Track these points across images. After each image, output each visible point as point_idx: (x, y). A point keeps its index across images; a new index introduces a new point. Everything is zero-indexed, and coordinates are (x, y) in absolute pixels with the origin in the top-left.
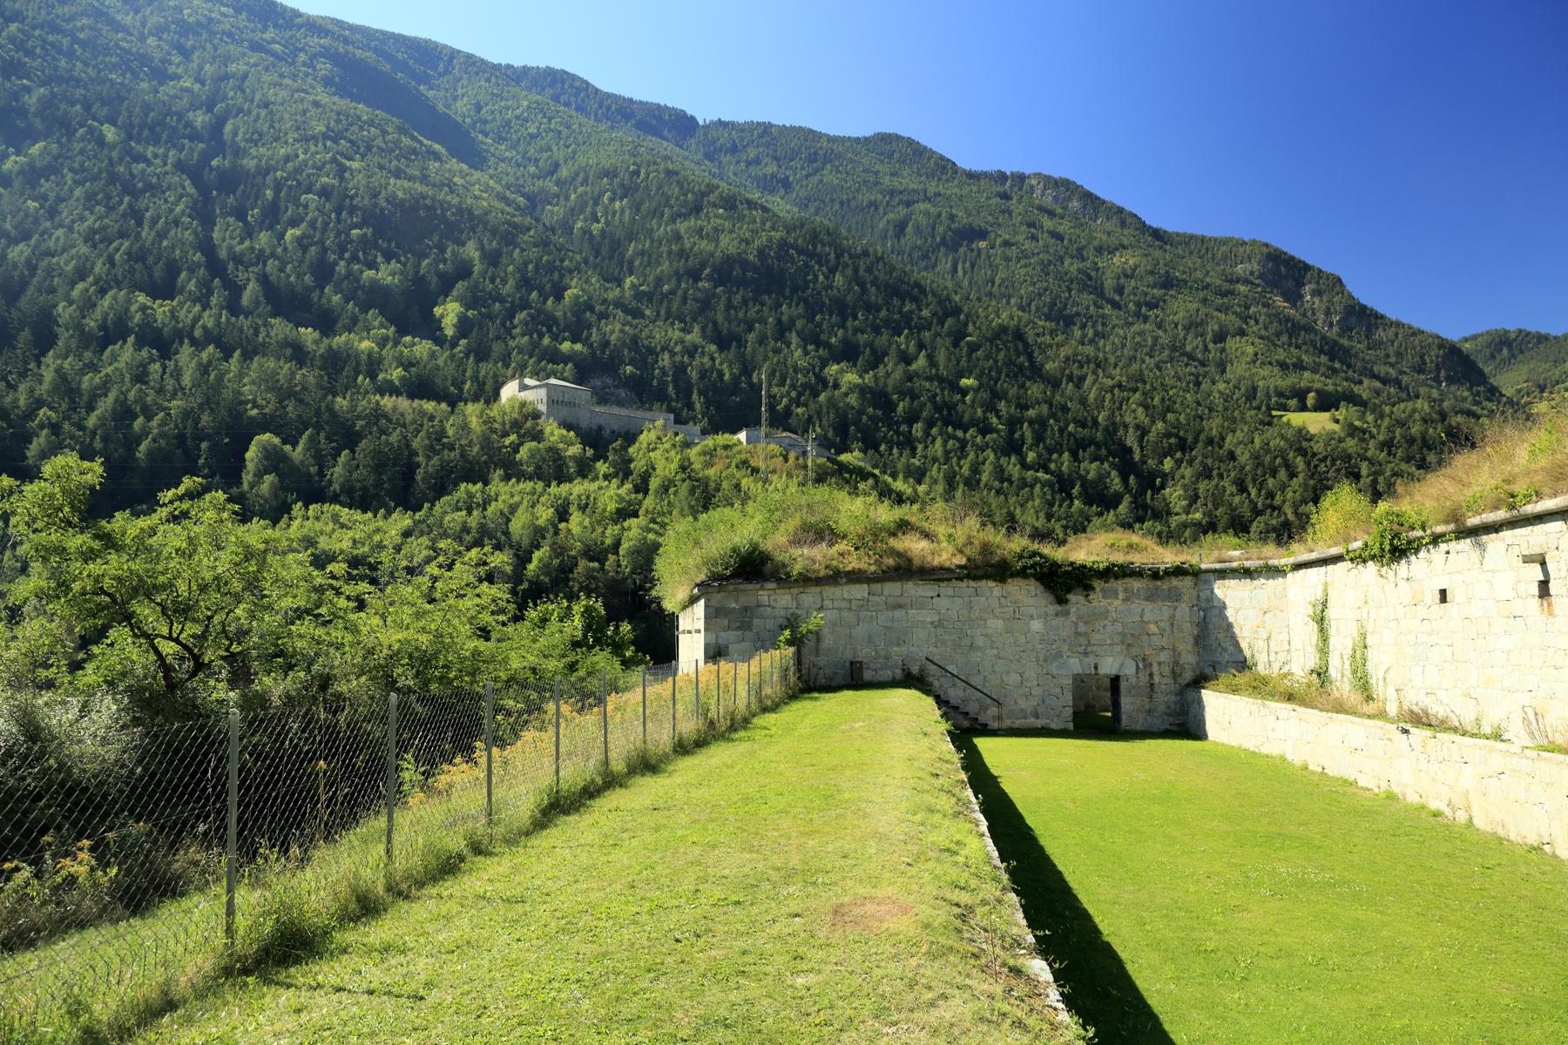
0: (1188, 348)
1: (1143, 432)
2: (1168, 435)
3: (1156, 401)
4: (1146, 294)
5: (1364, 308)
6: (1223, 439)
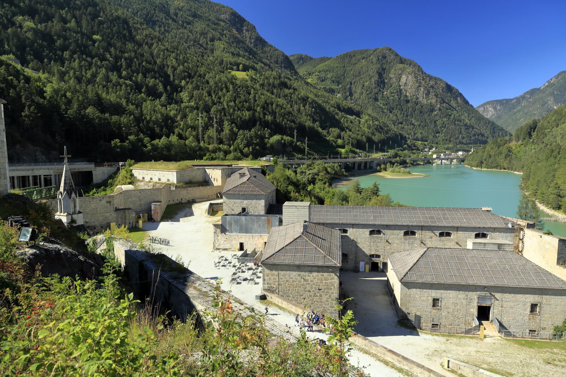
0: (201, 42)
1: (175, 69)
2: (184, 71)
3: (181, 58)
4: (186, 18)
5: (261, 38)
6: (205, 75)
